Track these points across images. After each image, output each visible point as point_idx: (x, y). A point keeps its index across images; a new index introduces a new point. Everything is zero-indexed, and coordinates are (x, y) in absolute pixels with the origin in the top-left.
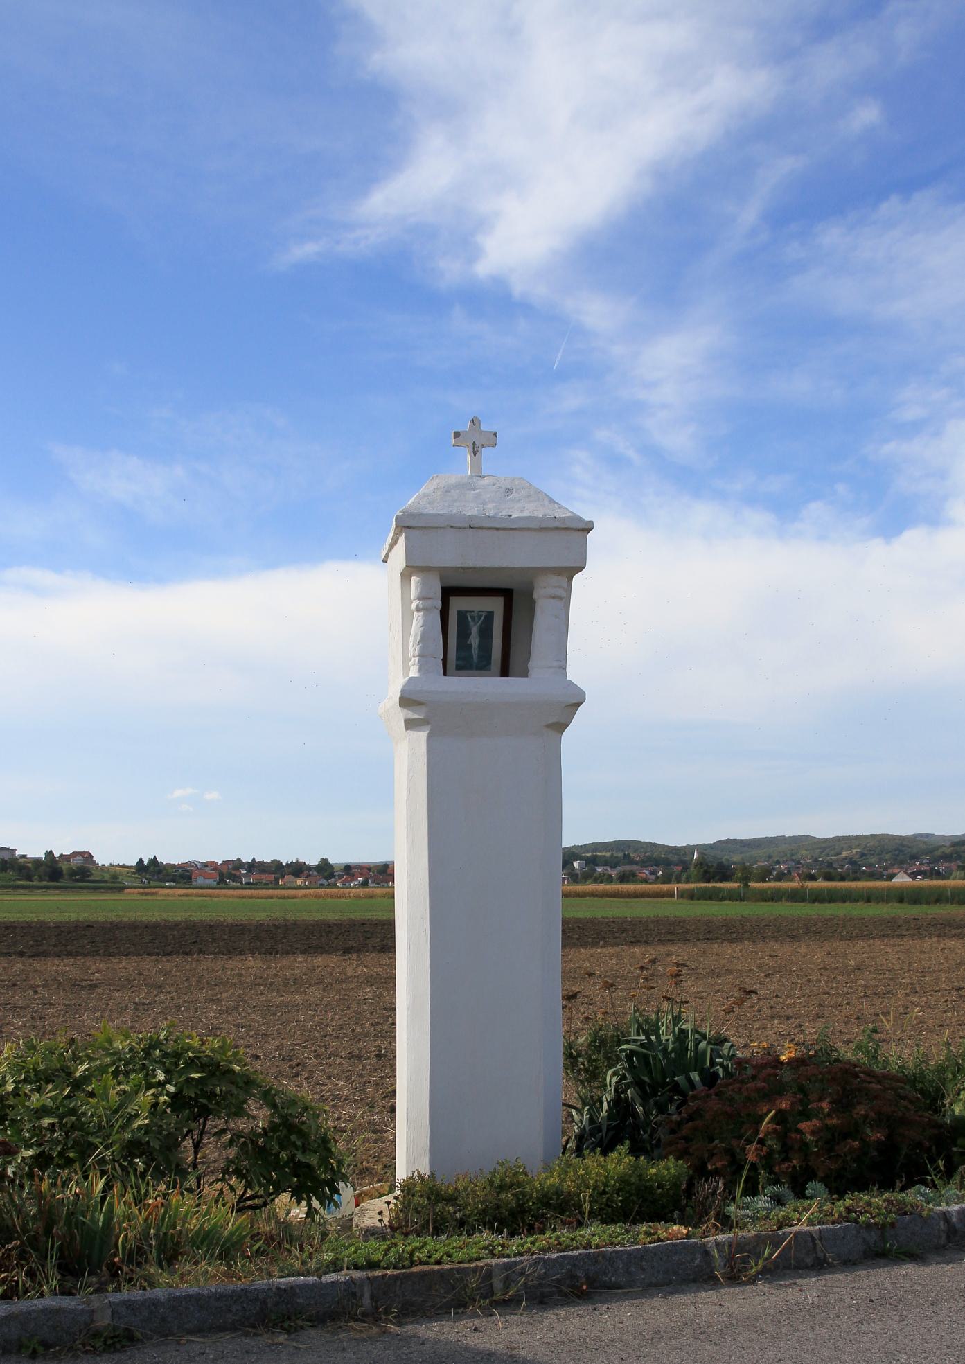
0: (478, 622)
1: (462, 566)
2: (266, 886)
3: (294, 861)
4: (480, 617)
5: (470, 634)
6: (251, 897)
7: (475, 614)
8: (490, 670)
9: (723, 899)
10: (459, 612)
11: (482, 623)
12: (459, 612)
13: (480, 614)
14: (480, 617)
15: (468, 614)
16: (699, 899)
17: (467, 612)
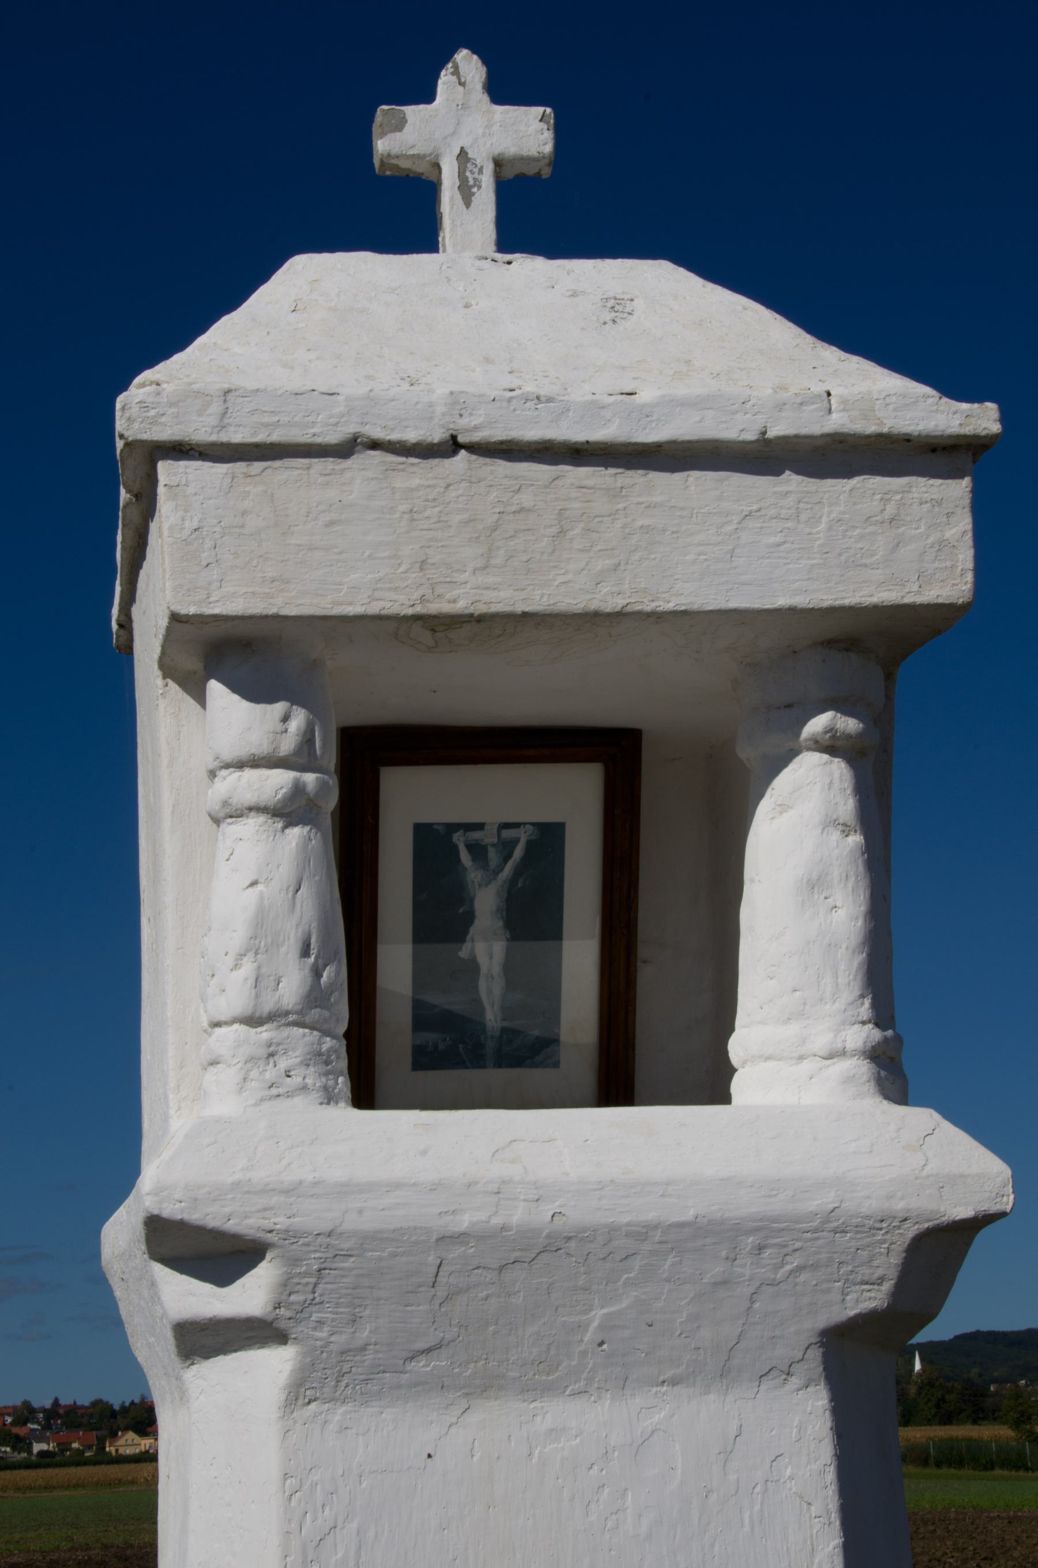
0: (500, 868)
1: (434, 608)
2: (79, 1460)
3: (137, 1400)
4: (507, 848)
5: (469, 918)
6: (48, 1488)
7: (488, 837)
8: (556, 1065)
9: (989, 1466)
10: (423, 832)
11: (518, 872)
12: (423, 832)
13: (507, 834)
14: (507, 848)
15: (459, 839)
16: (938, 1465)
17: (453, 827)
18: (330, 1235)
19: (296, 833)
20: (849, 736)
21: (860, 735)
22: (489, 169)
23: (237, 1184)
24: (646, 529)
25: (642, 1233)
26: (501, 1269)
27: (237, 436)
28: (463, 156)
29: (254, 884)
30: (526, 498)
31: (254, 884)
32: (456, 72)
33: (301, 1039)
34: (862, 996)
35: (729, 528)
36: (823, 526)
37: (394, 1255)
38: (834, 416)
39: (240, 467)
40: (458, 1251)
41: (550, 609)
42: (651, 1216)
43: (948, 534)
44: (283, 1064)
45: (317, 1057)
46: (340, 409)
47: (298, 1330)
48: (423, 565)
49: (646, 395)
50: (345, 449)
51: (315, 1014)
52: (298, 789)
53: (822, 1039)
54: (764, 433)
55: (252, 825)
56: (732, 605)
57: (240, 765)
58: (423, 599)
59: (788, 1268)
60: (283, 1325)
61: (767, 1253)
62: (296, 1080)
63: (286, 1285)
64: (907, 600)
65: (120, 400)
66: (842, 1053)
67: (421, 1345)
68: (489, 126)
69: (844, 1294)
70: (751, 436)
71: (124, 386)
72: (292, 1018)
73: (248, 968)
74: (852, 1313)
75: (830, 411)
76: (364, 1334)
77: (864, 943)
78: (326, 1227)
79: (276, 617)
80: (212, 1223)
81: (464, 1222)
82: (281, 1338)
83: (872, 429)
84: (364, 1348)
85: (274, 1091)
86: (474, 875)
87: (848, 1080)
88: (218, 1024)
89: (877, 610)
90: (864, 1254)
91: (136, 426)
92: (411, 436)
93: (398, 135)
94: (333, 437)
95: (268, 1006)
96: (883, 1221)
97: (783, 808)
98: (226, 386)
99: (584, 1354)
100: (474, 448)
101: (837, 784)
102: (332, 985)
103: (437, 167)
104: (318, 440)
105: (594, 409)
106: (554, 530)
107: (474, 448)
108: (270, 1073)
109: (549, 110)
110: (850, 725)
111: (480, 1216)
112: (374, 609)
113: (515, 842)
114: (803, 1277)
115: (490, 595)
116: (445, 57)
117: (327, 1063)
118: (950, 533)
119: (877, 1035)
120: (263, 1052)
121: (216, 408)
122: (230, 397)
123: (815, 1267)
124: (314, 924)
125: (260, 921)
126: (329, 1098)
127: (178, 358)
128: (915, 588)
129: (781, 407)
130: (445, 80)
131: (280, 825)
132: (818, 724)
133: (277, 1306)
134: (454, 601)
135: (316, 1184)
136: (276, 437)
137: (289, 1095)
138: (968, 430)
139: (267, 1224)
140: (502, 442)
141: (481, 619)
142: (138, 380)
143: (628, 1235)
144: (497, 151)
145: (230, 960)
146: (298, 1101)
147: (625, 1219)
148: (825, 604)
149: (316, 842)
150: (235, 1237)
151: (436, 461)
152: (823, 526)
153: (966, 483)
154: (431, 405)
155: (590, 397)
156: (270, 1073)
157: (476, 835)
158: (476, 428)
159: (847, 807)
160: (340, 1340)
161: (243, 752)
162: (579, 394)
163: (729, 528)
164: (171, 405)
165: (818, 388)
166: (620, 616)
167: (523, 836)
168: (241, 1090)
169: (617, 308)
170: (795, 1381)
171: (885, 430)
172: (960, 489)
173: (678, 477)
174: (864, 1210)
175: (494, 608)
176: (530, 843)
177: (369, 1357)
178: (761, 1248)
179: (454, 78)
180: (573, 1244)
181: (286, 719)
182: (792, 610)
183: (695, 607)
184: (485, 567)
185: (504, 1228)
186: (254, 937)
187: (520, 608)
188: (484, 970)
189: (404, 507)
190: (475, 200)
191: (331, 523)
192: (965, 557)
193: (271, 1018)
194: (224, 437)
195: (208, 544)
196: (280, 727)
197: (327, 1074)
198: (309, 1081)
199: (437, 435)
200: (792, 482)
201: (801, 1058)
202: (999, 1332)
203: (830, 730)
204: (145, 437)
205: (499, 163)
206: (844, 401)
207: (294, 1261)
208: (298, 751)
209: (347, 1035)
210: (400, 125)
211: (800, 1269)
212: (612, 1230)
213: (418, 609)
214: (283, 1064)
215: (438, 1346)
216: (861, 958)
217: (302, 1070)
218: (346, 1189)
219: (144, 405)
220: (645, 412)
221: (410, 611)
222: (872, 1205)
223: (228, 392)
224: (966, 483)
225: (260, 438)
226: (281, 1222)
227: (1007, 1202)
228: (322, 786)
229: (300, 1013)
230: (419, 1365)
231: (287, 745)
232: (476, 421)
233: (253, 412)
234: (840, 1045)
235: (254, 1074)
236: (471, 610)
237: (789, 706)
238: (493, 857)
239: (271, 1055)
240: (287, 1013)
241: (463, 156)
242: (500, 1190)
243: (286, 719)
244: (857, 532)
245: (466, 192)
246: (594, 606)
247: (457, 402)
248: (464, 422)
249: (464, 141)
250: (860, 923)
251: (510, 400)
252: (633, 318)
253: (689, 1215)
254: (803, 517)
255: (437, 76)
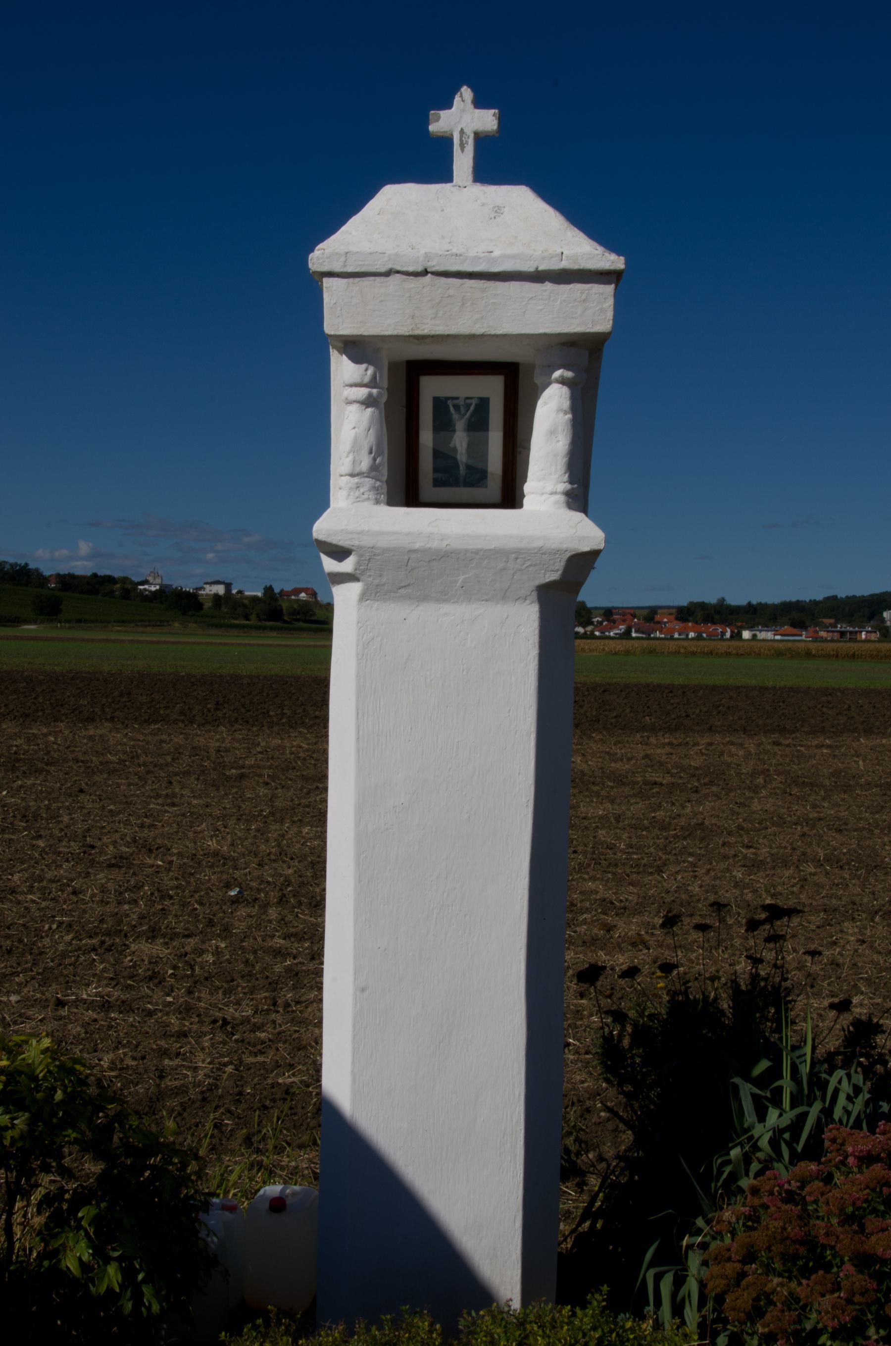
0: (465, 414)
4: (468, 407)
7: (461, 402)
11: (472, 416)
13: (468, 401)
14: (468, 407)
15: (450, 403)
17: (447, 399)
18: (372, 548)
19: (370, 410)
20: (569, 379)
21: (573, 378)
22: (472, 136)
23: (342, 530)
24: (494, 303)
25: (476, 552)
26: (429, 562)
27: (350, 269)
28: (462, 132)
29: (354, 428)
30: (451, 292)
31: (354, 428)
32: (461, 96)
33: (369, 482)
34: (565, 473)
35: (524, 303)
36: (558, 303)
37: (393, 555)
38: (563, 262)
39: (351, 280)
40: (414, 556)
41: (457, 333)
42: (480, 547)
43: (605, 306)
44: (362, 490)
45: (374, 488)
46: (386, 259)
47: (362, 578)
48: (413, 317)
49: (496, 254)
50: (388, 273)
51: (373, 473)
52: (370, 395)
53: (550, 487)
54: (537, 268)
55: (354, 407)
56: (523, 332)
57: (351, 386)
58: (412, 329)
59: (526, 565)
60: (358, 576)
61: (519, 560)
62: (366, 496)
63: (358, 563)
64: (588, 331)
65: (311, 256)
66: (555, 493)
67: (403, 584)
68: (472, 119)
69: (545, 574)
70: (532, 270)
71: (313, 251)
72: (365, 475)
73: (351, 458)
74: (547, 580)
75: (562, 260)
76: (384, 580)
77: (568, 454)
78: (371, 545)
79: (361, 336)
80: (334, 542)
81: (417, 546)
82: (357, 579)
83: (576, 267)
84: (384, 584)
85: (358, 500)
86: (455, 416)
87: (557, 502)
88: (341, 476)
89: (576, 334)
90: (552, 562)
91: (315, 266)
92: (411, 269)
93: (436, 124)
94: (383, 270)
95: (357, 470)
96: (558, 551)
97: (545, 403)
98: (347, 251)
99: (457, 590)
100: (434, 273)
101: (564, 396)
102: (380, 464)
103: (452, 135)
104: (378, 271)
105: (476, 259)
106: (460, 304)
107: (434, 273)
108: (357, 493)
109: (497, 111)
110: (569, 374)
111: (422, 544)
112: (395, 333)
113: (471, 404)
114: (531, 569)
115: (437, 328)
116: (456, 89)
117: (377, 490)
118: (605, 306)
119: (569, 486)
120: (355, 486)
121: (343, 259)
122: (348, 255)
123: (535, 565)
124: (374, 443)
125: (355, 441)
126: (377, 502)
127: (333, 237)
128: (591, 326)
129: (543, 258)
130: (457, 99)
131: (364, 407)
132: (557, 374)
133: (356, 570)
134: (423, 330)
135: (368, 531)
136: (363, 269)
137: (363, 501)
138: (612, 268)
139: (352, 543)
140: (443, 272)
141: (433, 336)
142: (317, 248)
143: (472, 552)
144: (475, 129)
145: (345, 454)
146: (366, 503)
147: (471, 547)
148: (557, 332)
149: (377, 413)
150: (342, 547)
151: (420, 278)
152: (558, 303)
153: (612, 286)
154: (418, 257)
155: (476, 254)
156: (357, 493)
157: (456, 402)
158: (434, 266)
159: (566, 404)
160: (376, 582)
161: (352, 381)
162: (471, 254)
163: (524, 303)
164: (327, 258)
165: (559, 251)
166: (482, 336)
167: (474, 402)
168: (347, 499)
169: (498, 211)
170: (527, 602)
171: (581, 268)
172: (610, 289)
173: (507, 284)
174: (552, 547)
175: (437, 333)
176: (476, 405)
177: (386, 587)
178: (517, 559)
179: (460, 99)
180: (453, 555)
181: (366, 370)
182: (545, 335)
183: (509, 333)
184: (435, 318)
185: (430, 548)
186: (353, 447)
187: (447, 333)
188: (459, 451)
189: (407, 295)
190: (465, 150)
191: (382, 301)
192: (610, 314)
193: (358, 475)
194: (345, 270)
195: (339, 309)
196: (364, 373)
197: (377, 494)
198: (370, 496)
199: (420, 269)
200: (548, 286)
201: (543, 494)
202: (766, 604)
203: (562, 376)
204: (318, 270)
205: (477, 134)
206: (567, 256)
207: (361, 556)
208: (371, 381)
209: (387, 481)
210: (438, 119)
211: (530, 566)
212: (466, 551)
213: (411, 333)
214: (362, 490)
215: (408, 585)
216: (566, 460)
217: (368, 493)
218: (379, 534)
219: (318, 258)
220: (495, 260)
221: (408, 334)
222: (555, 545)
223: (347, 253)
224: (612, 286)
225: (357, 270)
226: (357, 543)
227: (602, 546)
228: (379, 394)
229: (368, 473)
230: (402, 591)
231: (367, 379)
232: (434, 263)
233: (355, 261)
234: (555, 490)
235: (352, 493)
236: (429, 333)
237: (549, 366)
238: (462, 410)
239: (358, 487)
240: (363, 473)
241: (462, 132)
242: (430, 536)
243: (366, 370)
244: (571, 305)
245: (462, 147)
246: (473, 332)
247: (428, 256)
248: (429, 264)
249: (462, 125)
250: (567, 447)
251: (446, 255)
252: (502, 216)
253: (493, 547)
254: (552, 299)
255: (454, 98)
